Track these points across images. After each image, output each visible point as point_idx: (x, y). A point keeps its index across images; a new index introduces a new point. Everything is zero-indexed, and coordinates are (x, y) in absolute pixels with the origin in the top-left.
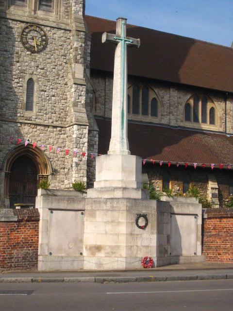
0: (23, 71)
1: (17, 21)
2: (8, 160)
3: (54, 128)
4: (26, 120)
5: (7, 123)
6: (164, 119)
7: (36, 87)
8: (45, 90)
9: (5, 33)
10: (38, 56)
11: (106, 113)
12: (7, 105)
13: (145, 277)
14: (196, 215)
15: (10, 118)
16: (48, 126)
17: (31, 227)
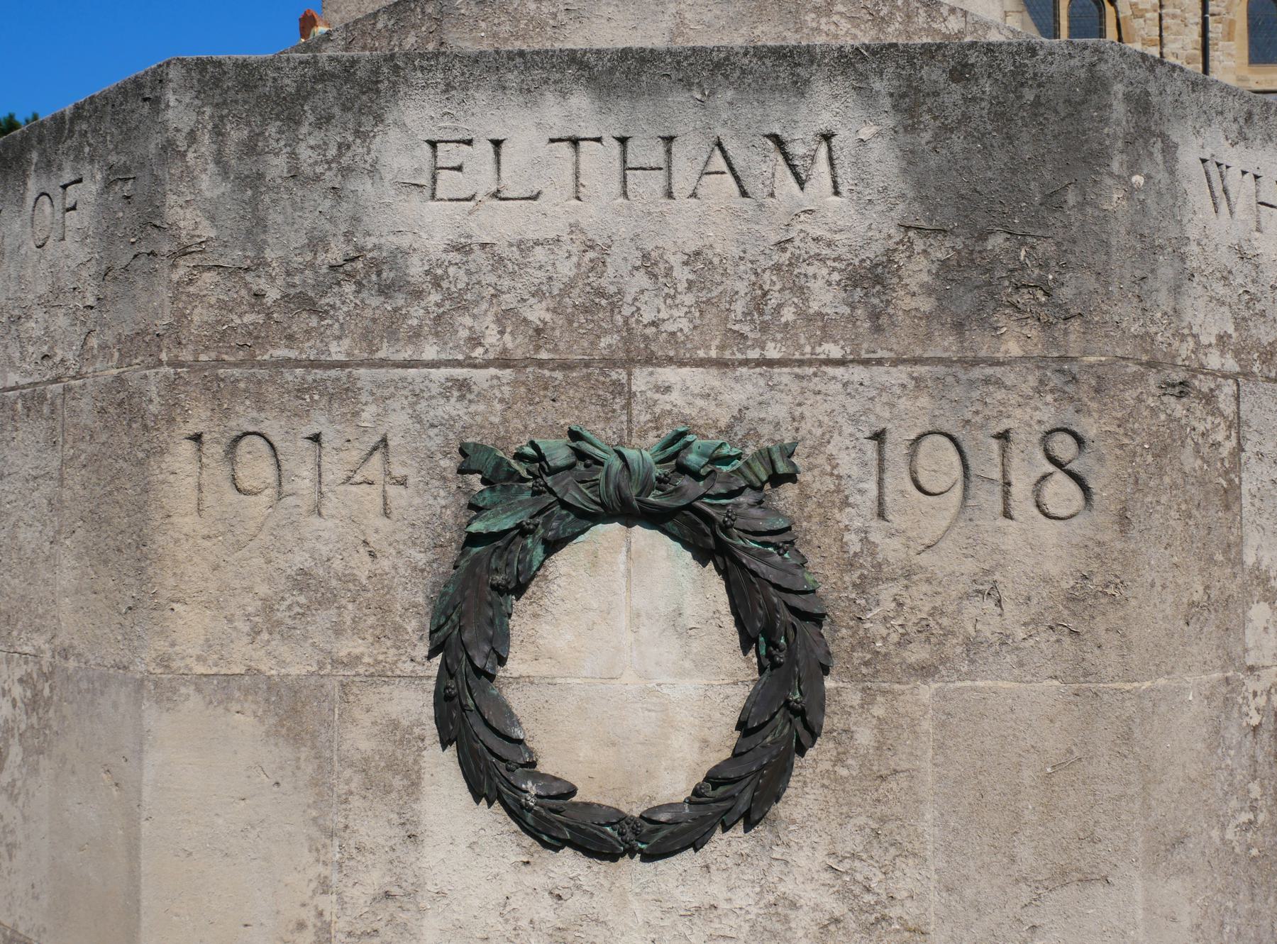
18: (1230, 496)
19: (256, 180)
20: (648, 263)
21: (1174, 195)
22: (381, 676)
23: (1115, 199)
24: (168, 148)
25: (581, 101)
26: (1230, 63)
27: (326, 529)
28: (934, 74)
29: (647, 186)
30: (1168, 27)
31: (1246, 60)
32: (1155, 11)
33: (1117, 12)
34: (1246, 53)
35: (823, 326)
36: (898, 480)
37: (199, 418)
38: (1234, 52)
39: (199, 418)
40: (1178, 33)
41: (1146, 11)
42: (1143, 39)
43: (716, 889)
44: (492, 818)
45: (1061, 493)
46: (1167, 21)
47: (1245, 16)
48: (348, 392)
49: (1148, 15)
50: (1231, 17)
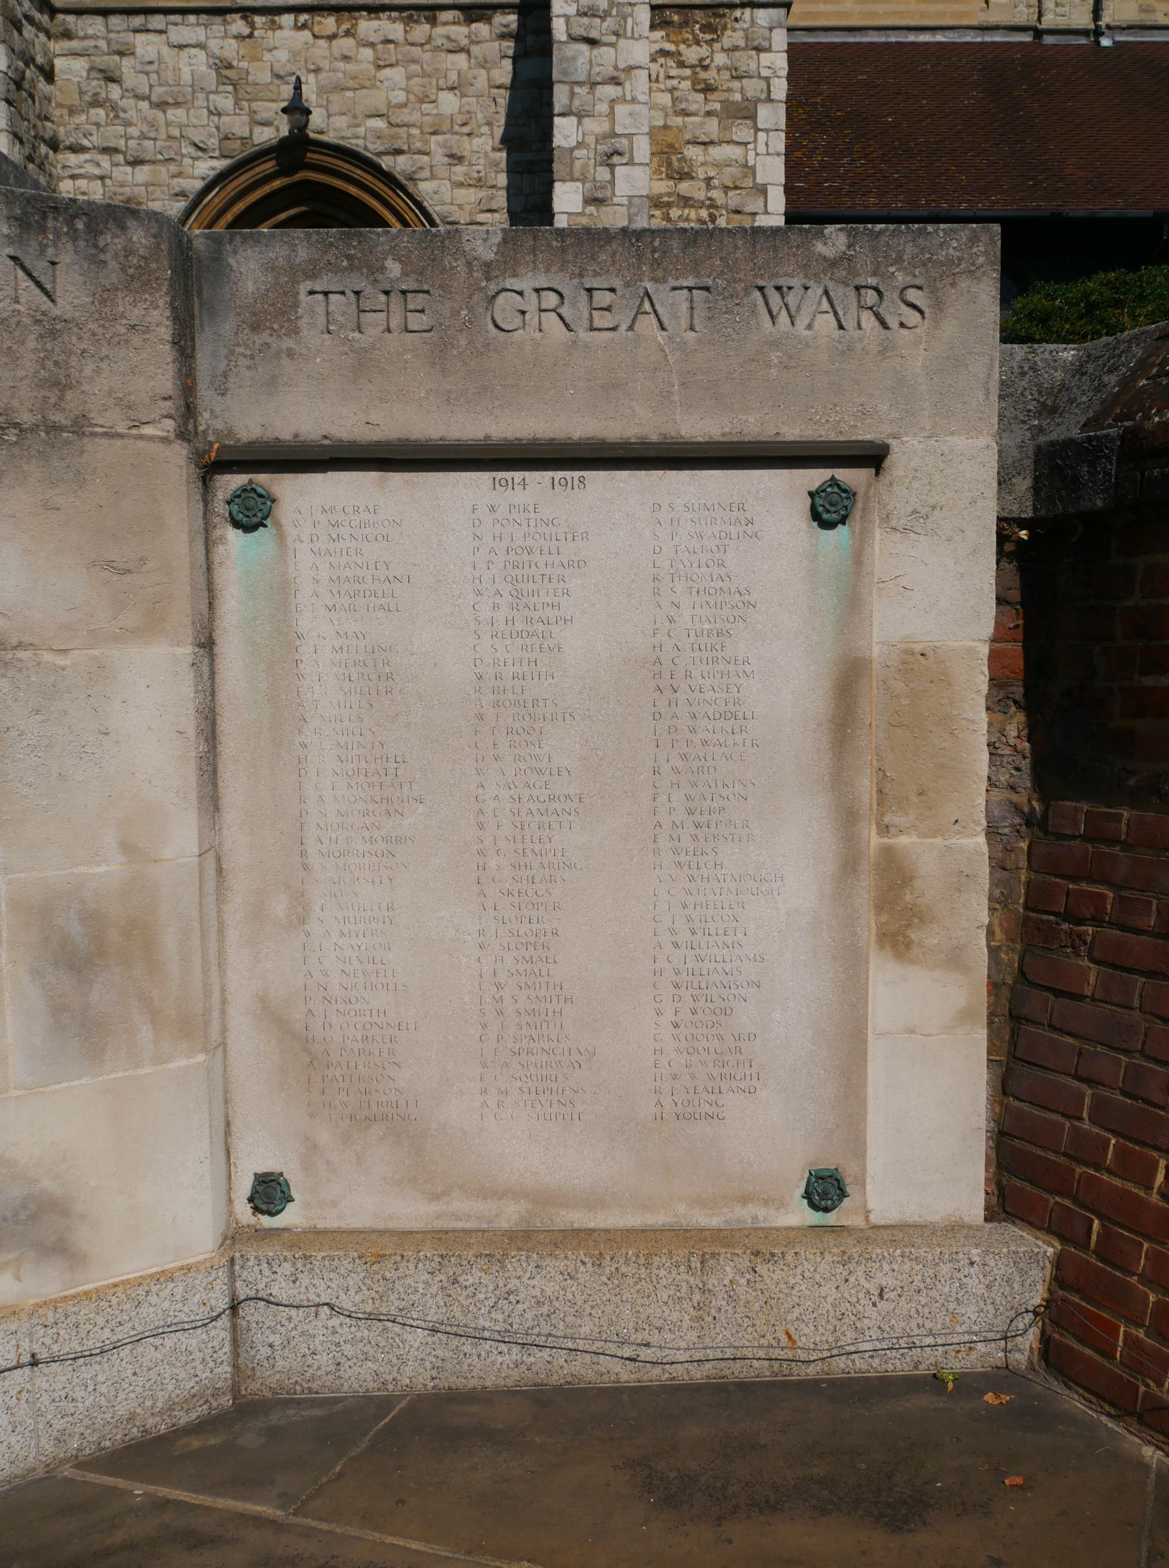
3: (470, 21)
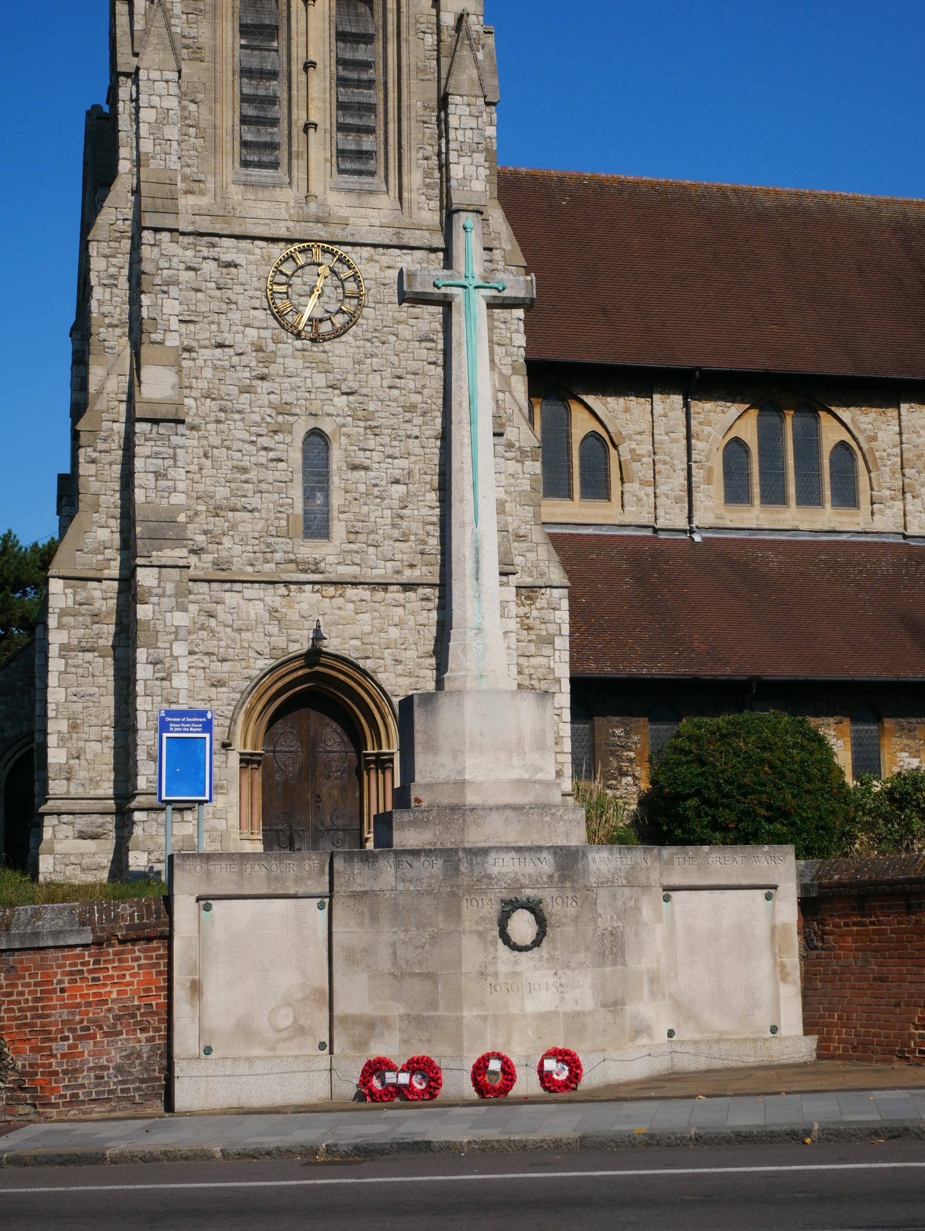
0: (283, 409)
1: (254, 238)
2: (249, 713)
3: (405, 591)
4: (304, 571)
5: (238, 586)
6: (881, 512)
7: (337, 457)
8: (367, 462)
9: (213, 285)
10: (336, 348)
11: (660, 512)
12: (233, 527)
13: (484, 1138)
14: (770, 890)
15: (250, 569)
16: (385, 586)
17: (143, 962)
18: (595, 904)
19: (472, 864)
20: (523, 875)
21: (588, 864)
22: (492, 930)
23: (580, 866)
24: (459, 860)
25: (514, 853)
26: (709, 503)
27: (484, 911)
28: (558, 850)
29: (522, 865)
30: (659, 472)
31: (722, 501)
32: (650, 456)
33: (619, 455)
34: (722, 494)
35: (545, 883)
36: (555, 903)
37: (467, 897)
38: (712, 494)
39: (467, 897)
40: (668, 477)
41: (643, 456)
42: (640, 480)
43: (534, 955)
44: (506, 947)
45: (574, 904)
46: (659, 467)
47: (721, 463)
48: (486, 893)
49: (644, 460)
50: (709, 464)
